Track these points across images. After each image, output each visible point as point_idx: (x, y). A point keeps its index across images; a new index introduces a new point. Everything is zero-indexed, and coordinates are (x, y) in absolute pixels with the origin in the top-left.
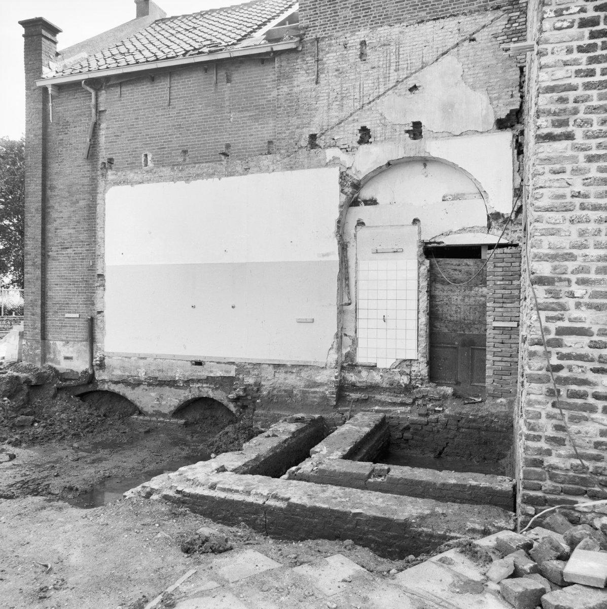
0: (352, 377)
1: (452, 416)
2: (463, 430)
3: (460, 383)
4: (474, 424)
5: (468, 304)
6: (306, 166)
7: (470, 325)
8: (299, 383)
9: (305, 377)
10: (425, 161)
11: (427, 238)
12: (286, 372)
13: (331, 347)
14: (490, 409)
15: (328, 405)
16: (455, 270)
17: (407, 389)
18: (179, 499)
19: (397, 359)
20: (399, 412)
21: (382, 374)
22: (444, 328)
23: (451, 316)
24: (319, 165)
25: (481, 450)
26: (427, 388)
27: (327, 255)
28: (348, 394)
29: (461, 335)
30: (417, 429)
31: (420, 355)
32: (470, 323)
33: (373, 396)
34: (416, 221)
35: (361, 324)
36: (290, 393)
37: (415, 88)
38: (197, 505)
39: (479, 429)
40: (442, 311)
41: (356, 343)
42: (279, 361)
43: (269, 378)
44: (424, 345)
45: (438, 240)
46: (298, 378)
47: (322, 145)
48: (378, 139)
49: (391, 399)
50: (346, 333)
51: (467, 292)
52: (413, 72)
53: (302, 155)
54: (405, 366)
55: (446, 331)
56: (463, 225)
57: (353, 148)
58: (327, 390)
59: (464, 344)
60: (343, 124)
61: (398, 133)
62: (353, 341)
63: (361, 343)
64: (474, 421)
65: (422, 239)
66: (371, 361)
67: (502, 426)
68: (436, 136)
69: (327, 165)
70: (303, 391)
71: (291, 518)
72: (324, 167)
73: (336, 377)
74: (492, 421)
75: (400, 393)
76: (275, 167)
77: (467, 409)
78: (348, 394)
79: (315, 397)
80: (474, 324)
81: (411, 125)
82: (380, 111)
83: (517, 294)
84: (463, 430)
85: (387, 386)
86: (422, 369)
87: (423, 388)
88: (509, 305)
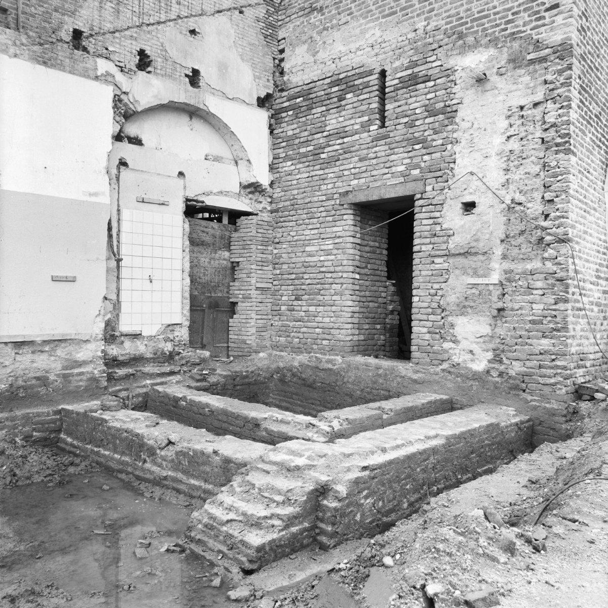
1: (230, 376)
3: (205, 345)
6: (68, 68)
8: (53, 366)
9: (63, 355)
10: (193, 112)
11: (191, 195)
12: (33, 352)
13: (98, 313)
15: (97, 387)
16: (203, 231)
18: (369, 477)
21: (146, 342)
23: (200, 278)
24: (85, 74)
27: (95, 194)
31: (185, 318)
33: (138, 369)
34: (181, 174)
36: (43, 380)
37: (193, 32)
39: (249, 384)
42: (24, 336)
43: (7, 363)
45: (200, 198)
46: (53, 358)
47: (91, 49)
48: (159, 71)
49: (158, 370)
51: (213, 255)
52: (194, 14)
53: (63, 51)
55: (197, 293)
56: (222, 189)
57: (130, 70)
58: (96, 369)
59: (210, 307)
60: (117, 34)
61: (178, 74)
63: (124, 307)
64: (247, 377)
65: (187, 195)
66: (135, 329)
67: (265, 378)
68: (214, 91)
69: (97, 78)
72: (93, 79)
76: (18, 52)
77: (238, 367)
79: (81, 380)
80: (219, 286)
81: (191, 70)
82: (161, 40)
85: (152, 356)
86: (183, 334)
87: (184, 354)
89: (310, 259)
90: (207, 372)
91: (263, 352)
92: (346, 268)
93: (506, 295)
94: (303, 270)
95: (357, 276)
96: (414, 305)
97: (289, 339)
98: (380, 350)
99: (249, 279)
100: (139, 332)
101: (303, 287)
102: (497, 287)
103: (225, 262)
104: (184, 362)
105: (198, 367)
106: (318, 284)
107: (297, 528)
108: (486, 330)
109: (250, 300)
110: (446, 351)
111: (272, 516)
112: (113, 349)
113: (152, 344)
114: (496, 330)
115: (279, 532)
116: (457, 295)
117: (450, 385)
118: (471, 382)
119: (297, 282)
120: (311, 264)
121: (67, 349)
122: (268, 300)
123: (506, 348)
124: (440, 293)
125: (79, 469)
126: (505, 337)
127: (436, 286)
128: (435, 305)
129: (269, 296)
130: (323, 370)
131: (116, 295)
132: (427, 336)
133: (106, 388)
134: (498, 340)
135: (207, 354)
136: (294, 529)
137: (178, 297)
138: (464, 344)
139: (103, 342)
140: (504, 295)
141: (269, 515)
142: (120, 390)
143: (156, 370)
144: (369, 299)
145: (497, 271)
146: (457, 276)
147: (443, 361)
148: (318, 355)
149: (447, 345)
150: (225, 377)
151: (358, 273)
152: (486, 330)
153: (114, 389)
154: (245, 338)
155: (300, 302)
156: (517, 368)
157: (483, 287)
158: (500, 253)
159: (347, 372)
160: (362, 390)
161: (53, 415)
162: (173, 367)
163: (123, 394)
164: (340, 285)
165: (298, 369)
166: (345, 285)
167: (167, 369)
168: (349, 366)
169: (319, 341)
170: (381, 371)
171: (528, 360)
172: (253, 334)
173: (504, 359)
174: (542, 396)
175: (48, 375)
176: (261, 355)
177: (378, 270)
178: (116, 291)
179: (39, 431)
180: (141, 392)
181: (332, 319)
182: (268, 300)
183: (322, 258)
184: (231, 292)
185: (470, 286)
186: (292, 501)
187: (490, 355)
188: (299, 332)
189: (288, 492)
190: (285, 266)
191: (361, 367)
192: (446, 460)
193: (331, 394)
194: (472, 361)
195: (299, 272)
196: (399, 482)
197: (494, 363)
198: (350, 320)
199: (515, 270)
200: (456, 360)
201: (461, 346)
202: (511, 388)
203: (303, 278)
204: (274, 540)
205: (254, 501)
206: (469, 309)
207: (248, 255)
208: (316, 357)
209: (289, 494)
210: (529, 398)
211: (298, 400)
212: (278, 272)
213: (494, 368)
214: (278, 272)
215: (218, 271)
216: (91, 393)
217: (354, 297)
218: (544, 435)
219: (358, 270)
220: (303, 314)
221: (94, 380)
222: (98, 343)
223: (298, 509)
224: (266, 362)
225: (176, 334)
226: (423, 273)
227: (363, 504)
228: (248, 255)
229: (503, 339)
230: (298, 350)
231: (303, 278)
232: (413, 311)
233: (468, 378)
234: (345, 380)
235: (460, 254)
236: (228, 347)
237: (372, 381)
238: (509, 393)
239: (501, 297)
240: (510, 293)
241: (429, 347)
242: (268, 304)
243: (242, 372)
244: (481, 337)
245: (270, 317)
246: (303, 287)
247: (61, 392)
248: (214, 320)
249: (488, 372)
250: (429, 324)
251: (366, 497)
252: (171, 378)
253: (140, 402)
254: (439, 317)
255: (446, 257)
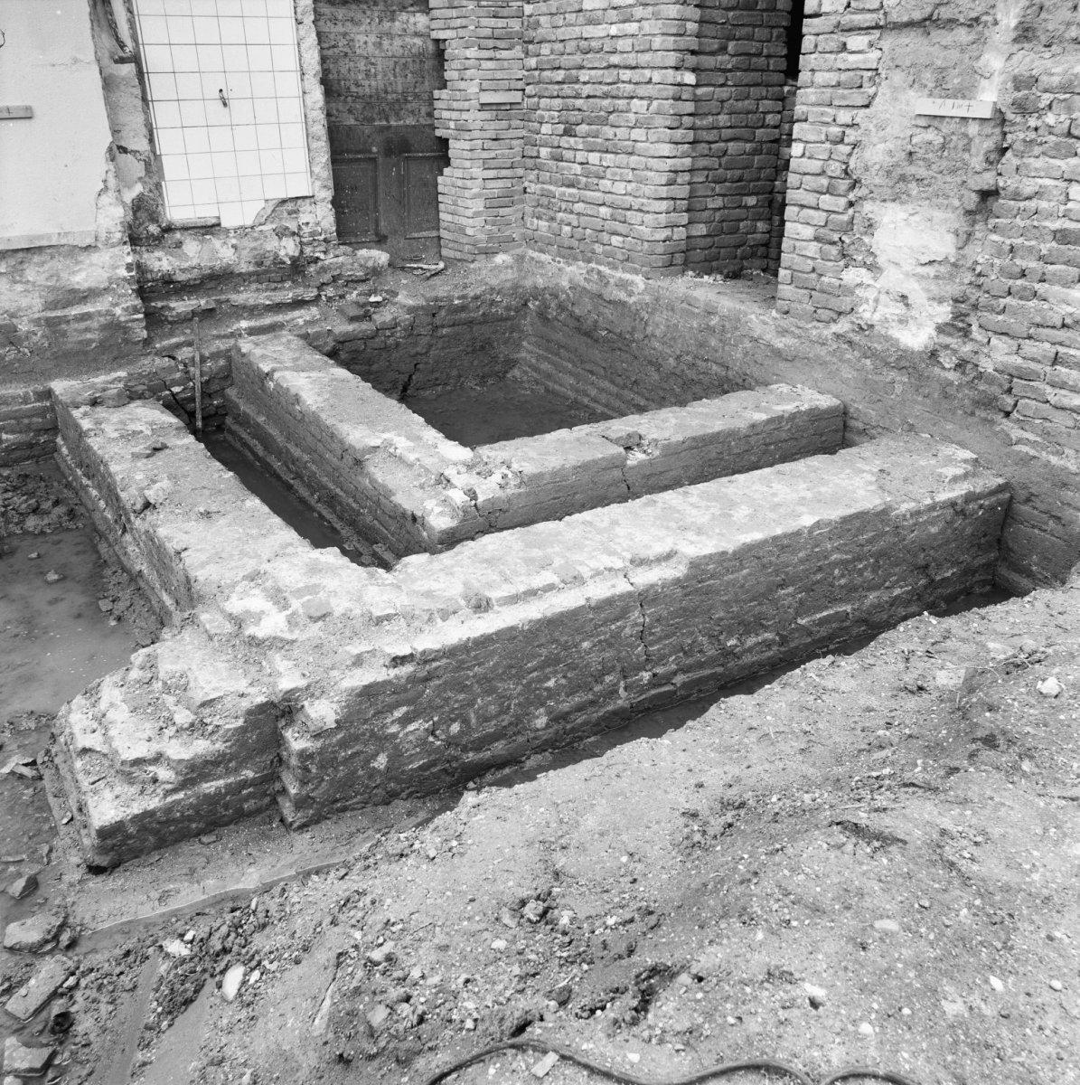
0: (161, 262)
2: (444, 331)
3: (385, 237)
4: (463, 315)
5: (390, 54)
7: (397, 106)
8: (24, 302)
9: (41, 280)
13: (101, 186)
14: (488, 280)
15: (126, 341)
17: (297, 267)
19: (267, 201)
20: (301, 322)
21: (234, 241)
22: (345, 115)
23: (357, 85)
25: (476, 363)
26: (336, 258)
28: (160, 304)
29: (382, 129)
30: (356, 351)
31: (318, 183)
32: (398, 100)
33: (223, 297)
35: (163, 115)
38: (469, 668)
39: (470, 323)
40: (338, 72)
41: (154, 168)
44: (324, 160)
46: (19, 287)
49: (268, 298)
50: (123, 144)
51: (387, 25)
54: (285, 214)
55: (352, 122)
59: (388, 151)
62: (147, 164)
63: (171, 167)
64: (463, 308)
66: (206, 214)
67: (508, 308)
70: (47, 320)
71: (697, 590)
73: (129, 267)
74: (493, 303)
75: (282, 281)
77: (442, 288)
78: (160, 304)
79: (87, 330)
80: (406, 101)
83: (517, 28)
84: (444, 331)
85: (251, 269)
86: (321, 217)
87: (329, 260)
88: (505, 54)
89: (590, 31)
90: (379, 299)
91: (505, 252)
92: (658, 58)
93: (1009, 154)
94: (578, 58)
95: (690, 78)
96: (793, 164)
97: (555, 225)
98: (753, 255)
99: (462, 85)
100: (214, 221)
101: (579, 103)
102: (988, 129)
103: (418, 41)
104: (326, 278)
105: (362, 288)
106: (606, 96)
107: (221, 783)
108: (943, 246)
109: (467, 135)
110: (849, 291)
111: (158, 759)
112: (160, 260)
113: (248, 243)
114: (967, 250)
115: (165, 796)
116: (890, 145)
117: (847, 373)
118: (893, 374)
119: (567, 90)
120: (594, 44)
121: (46, 267)
122: (512, 133)
123: (984, 299)
124: (852, 135)
125: (46, 521)
126: (986, 270)
127: (844, 117)
128: (835, 168)
129: (516, 123)
130: (610, 302)
131: (145, 142)
132: (812, 249)
133: (147, 342)
134: (968, 277)
135: (380, 257)
136: (209, 787)
137: (296, 135)
138: (892, 279)
139: (128, 248)
140: (1003, 151)
141: (149, 755)
142: (178, 346)
143: (264, 299)
144: (727, 133)
145: (997, 79)
146: (895, 89)
147: (840, 314)
148: (602, 268)
149: (852, 276)
150: (411, 310)
151: (694, 70)
152: (943, 246)
153: (166, 343)
154: (464, 221)
155: (572, 140)
156: (999, 355)
157: (953, 126)
158: (1013, 23)
159: (652, 314)
160: (678, 358)
161: (37, 401)
162: (300, 291)
163: (185, 353)
164: (645, 103)
165: (568, 295)
166: (655, 103)
167: (288, 295)
168: (657, 300)
169: (605, 237)
170: (714, 321)
171: (1030, 337)
172: (477, 214)
173: (974, 328)
174: (1046, 433)
175: (14, 321)
176: (500, 259)
177: (759, 55)
178: (144, 131)
179: (13, 432)
180: (222, 347)
181: (630, 187)
182: (512, 133)
183: (614, 30)
184: (436, 114)
185: (923, 122)
186: (210, 728)
187: (944, 313)
188: (572, 212)
189: (203, 705)
190: (545, 49)
191: (678, 306)
192: (687, 613)
193: (624, 356)
194: (901, 321)
195: (571, 64)
196: (519, 677)
197: (950, 335)
198: (664, 192)
199: (1044, 78)
200: (867, 315)
201: (882, 282)
202: (977, 403)
203: (577, 81)
204: (148, 814)
205: (145, 713)
206: (913, 185)
207: (458, 22)
208: (599, 272)
209: (207, 711)
210: (1016, 433)
211: (569, 360)
212: (532, 62)
213: (947, 347)
214: (532, 62)
215: (400, 64)
216: (116, 353)
217: (681, 131)
218: (1033, 527)
219: (691, 60)
220: (578, 169)
221: (114, 327)
222: (116, 250)
223: (220, 746)
224: (510, 275)
225: (303, 218)
226: (820, 78)
227: (395, 736)
228: (458, 22)
229: (980, 275)
230: (568, 253)
231: (577, 81)
232: (792, 179)
233: (887, 364)
234: (649, 329)
235: (910, 24)
236: (439, 238)
237: (696, 340)
238: (973, 414)
239: (993, 157)
240: (1018, 146)
241: (814, 276)
242: (514, 142)
243: (450, 299)
244: (931, 263)
245: (520, 172)
246: (579, 103)
247: (48, 354)
248: (402, 181)
249: (933, 354)
250: (819, 217)
251: (405, 721)
252: (296, 313)
253: (221, 368)
254: (843, 201)
255: (877, 33)
